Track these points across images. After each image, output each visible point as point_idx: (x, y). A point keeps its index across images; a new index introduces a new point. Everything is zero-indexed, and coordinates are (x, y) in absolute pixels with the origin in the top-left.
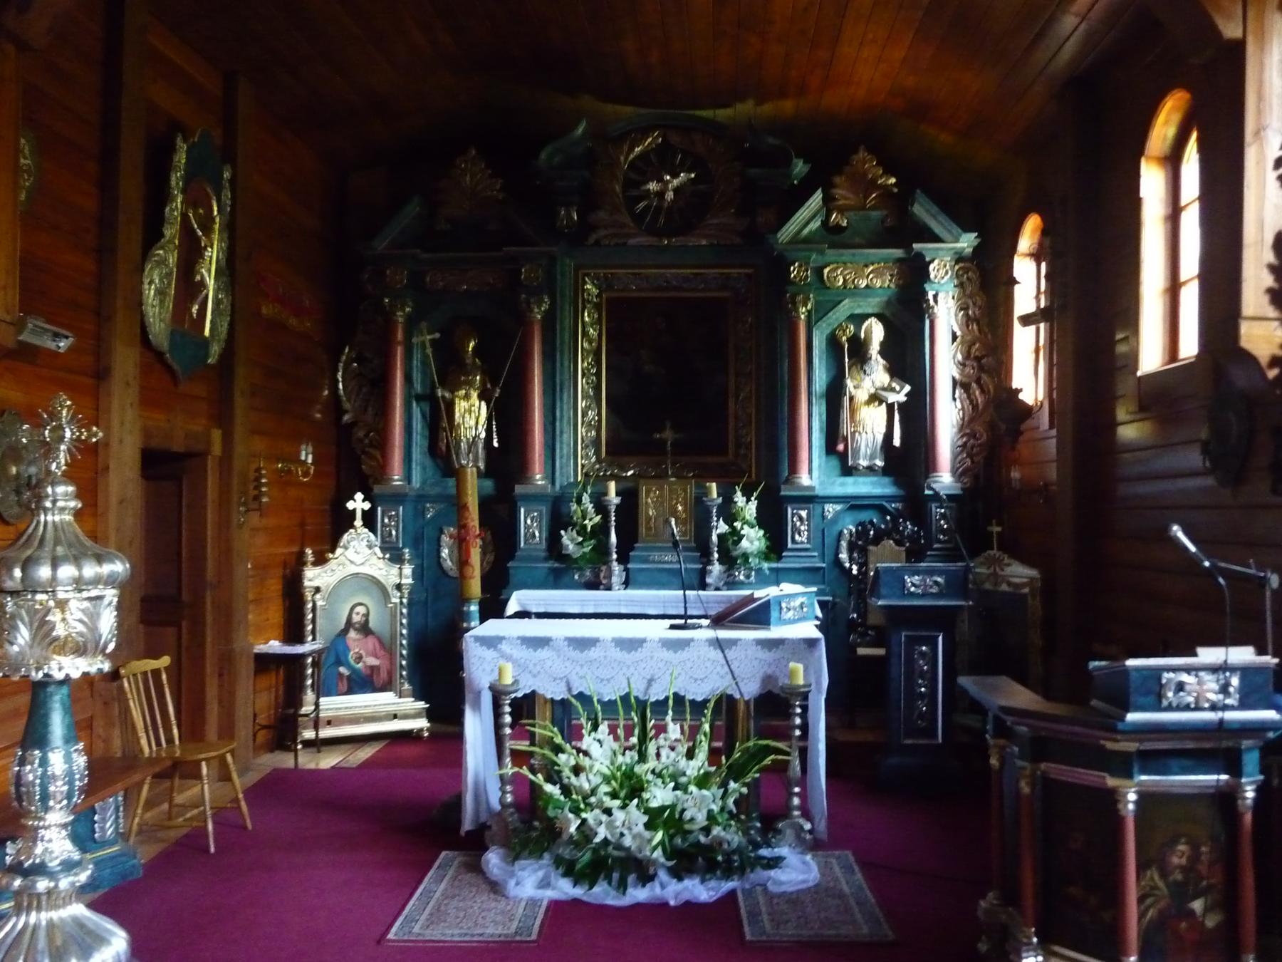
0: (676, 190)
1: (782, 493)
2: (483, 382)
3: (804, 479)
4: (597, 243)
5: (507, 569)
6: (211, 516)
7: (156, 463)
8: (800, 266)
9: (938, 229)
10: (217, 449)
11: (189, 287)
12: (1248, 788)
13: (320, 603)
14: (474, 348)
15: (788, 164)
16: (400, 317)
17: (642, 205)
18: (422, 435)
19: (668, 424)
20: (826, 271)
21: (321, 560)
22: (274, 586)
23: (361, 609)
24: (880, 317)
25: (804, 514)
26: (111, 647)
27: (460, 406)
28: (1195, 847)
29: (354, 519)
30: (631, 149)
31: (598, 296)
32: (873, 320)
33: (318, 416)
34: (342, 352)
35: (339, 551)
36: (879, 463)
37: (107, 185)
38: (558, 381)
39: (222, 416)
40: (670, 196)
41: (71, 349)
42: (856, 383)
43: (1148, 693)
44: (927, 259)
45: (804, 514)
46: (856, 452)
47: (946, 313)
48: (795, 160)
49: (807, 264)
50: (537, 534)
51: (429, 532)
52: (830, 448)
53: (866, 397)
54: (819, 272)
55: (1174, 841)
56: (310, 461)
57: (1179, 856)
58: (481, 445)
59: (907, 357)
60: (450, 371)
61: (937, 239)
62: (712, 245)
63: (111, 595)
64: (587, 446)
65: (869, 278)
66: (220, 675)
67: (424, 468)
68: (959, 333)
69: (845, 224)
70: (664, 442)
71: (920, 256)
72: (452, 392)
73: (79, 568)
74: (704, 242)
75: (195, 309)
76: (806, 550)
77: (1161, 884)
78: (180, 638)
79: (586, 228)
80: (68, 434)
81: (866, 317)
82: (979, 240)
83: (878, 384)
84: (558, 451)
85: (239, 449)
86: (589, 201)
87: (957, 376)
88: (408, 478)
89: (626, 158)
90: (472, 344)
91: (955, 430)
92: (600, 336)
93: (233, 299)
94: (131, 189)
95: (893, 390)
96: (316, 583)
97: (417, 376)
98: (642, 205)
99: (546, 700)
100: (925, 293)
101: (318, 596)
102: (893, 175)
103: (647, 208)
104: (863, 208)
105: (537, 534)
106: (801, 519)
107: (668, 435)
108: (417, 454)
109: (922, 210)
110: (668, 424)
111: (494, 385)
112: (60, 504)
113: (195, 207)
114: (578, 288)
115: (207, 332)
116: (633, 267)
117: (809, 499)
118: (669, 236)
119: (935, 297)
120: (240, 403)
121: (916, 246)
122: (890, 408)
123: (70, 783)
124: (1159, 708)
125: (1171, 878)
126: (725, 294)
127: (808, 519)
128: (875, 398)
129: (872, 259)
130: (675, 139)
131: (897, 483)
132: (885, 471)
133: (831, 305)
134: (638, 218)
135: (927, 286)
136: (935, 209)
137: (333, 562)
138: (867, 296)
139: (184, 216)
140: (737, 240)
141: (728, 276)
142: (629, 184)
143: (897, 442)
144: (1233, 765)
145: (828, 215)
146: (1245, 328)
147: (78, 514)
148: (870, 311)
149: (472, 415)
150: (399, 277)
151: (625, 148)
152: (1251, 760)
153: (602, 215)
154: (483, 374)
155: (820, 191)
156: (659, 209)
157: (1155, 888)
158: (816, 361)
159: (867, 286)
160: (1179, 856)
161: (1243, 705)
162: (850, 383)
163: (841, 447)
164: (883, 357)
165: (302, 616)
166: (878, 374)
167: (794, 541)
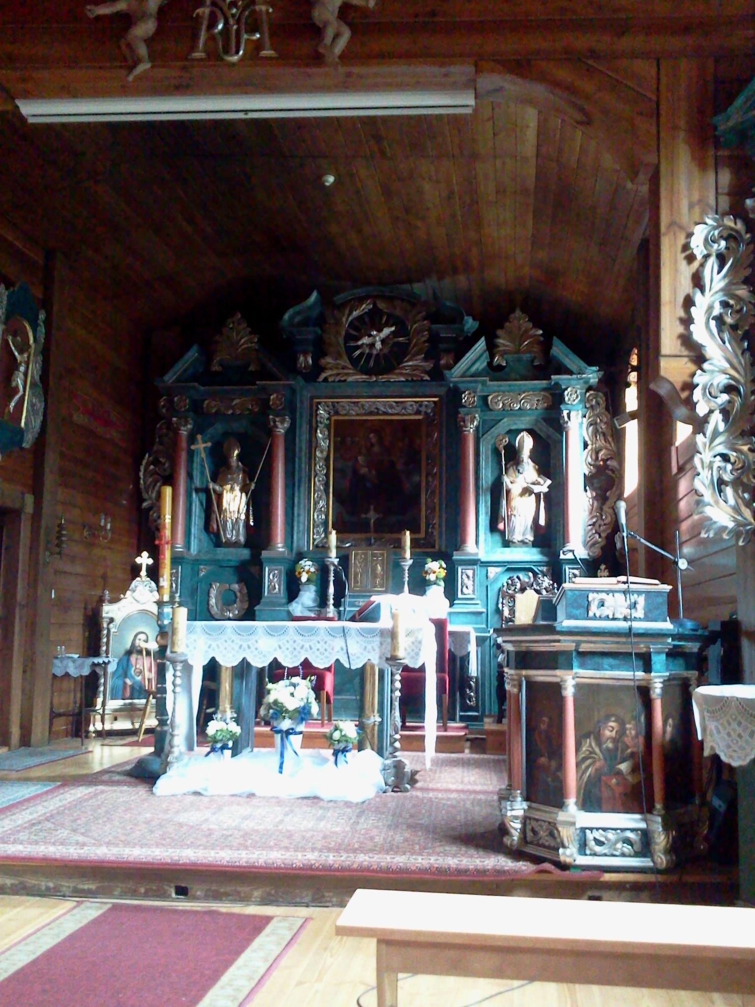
1: (454, 557)
2: (244, 480)
4: (326, 380)
5: (255, 611)
8: (470, 394)
9: (573, 367)
10: (29, 508)
12: (656, 680)
13: (113, 630)
14: (238, 455)
16: (184, 432)
17: (358, 352)
18: (200, 517)
20: (490, 398)
21: (115, 600)
22: (77, 617)
23: (142, 637)
24: (531, 432)
28: (622, 723)
29: (140, 570)
30: (350, 313)
31: (328, 419)
33: (124, 502)
34: (143, 458)
35: (128, 593)
40: (378, 345)
43: (579, 607)
44: (563, 387)
45: (470, 573)
46: (512, 531)
47: (578, 427)
48: (466, 318)
50: (277, 586)
51: (202, 587)
52: (493, 527)
53: (520, 490)
54: (484, 399)
55: (607, 718)
56: (109, 527)
57: (610, 731)
60: (220, 470)
64: (318, 526)
65: (524, 401)
67: (200, 540)
68: (589, 442)
69: (504, 364)
71: (557, 385)
72: (222, 486)
77: (597, 750)
79: (318, 368)
81: (519, 431)
82: (601, 373)
83: (530, 481)
84: (295, 528)
85: (46, 508)
86: (320, 350)
87: (587, 473)
88: (188, 545)
89: (347, 320)
90: (236, 452)
92: (329, 447)
95: (539, 484)
96: (110, 615)
97: (196, 474)
98: (358, 352)
100: (561, 412)
101: (111, 625)
102: (541, 328)
103: (362, 354)
104: (518, 352)
105: (277, 586)
106: (468, 577)
109: (559, 350)
111: (251, 480)
114: (313, 413)
116: (351, 397)
118: (377, 374)
119: (569, 415)
120: (50, 479)
122: (538, 496)
124: (587, 618)
125: (604, 746)
126: (420, 417)
128: (527, 491)
129: (524, 388)
130: (381, 305)
131: (542, 553)
132: (535, 544)
133: (494, 422)
134: (355, 362)
135: (562, 407)
136: (567, 350)
138: (520, 416)
140: (427, 378)
142: (348, 338)
143: (542, 522)
145: (492, 357)
146: (664, 363)
148: (523, 427)
149: (234, 502)
150: (182, 402)
151: (347, 312)
152: (659, 661)
153: (329, 360)
155: (483, 339)
156: (370, 355)
157: (593, 752)
161: (647, 618)
162: (506, 480)
163: (501, 526)
164: (533, 461)
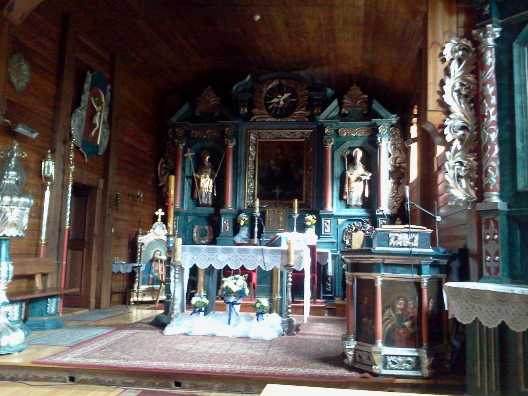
0: (284, 101)
2: (211, 172)
3: (329, 208)
4: (254, 120)
5: (216, 240)
6: (98, 210)
7: (78, 189)
9: (383, 114)
11: (90, 124)
13: (143, 249)
14: (209, 159)
15: (325, 90)
16: (181, 147)
19: (277, 186)
20: (340, 130)
21: (145, 234)
22: (125, 242)
24: (361, 148)
25: (329, 221)
26: (26, 228)
27: (203, 181)
28: (406, 301)
30: (267, 86)
32: (358, 149)
33: (150, 183)
34: (160, 161)
35: (151, 230)
36: (360, 203)
37: (58, 85)
38: (239, 172)
39: (105, 176)
40: (282, 103)
41: (36, 138)
42: (351, 173)
45: (329, 221)
46: (351, 200)
47: (386, 146)
48: (328, 89)
49: (332, 127)
53: (355, 178)
54: (337, 131)
55: (399, 298)
56: (142, 196)
57: (400, 305)
58: (210, 195)
59: (371, 163)
60: (199, 167)
61: (381, 117)
62: (296, 121)
63: (28, 210)
66: (98, 270)
67: (189, 203)
68: (392, 154)
69: (347, 113)
70: (275, 194)
71: (375, 124)
72: (200, 175)
73: (12, 198)
74: (294, 120)
75: (93, 132)
76: (329, 235)
77: (393, 315)
78: (83, 256)
79: (251, 114)
80: (15, 155)
81: (355, 148)
83: (360, 173)
85: (110, 187)
90: (208, 158)
91: (390, 191)
92: (256, 155)
93: (110, 133)
94: (68, 88)
95: (365, 175)
96: (142, 241)
98: (271, 107)
99: (202, 270)
103: (273, 107)
104: (355, 107)
106: (327, 223)
107: (278, 191)
108: (186, 198)
109: (376, 106)
110: (277, 186)
111: (215, 172)
112: (10, 177)
113: (95, 97)
114: (248, 138)
115: (98, 142)
117: (331, 216)
118: (281, 118)
120: (112, 170)
121: (373, 120)
123: (8, 274)
125: (397, 313)
126: (303, 140)
127: (330, 224)
128: (359, 179)
129: (358, 125)
130: (284, 82)
131: (367, 211)
132: (363, 207)
134: (269, 111)
137: (149, 234)
138: (356, 140)
139: (90, 102)
141: (303, 133)
142: (266, 99)
143: (367, 195)
144: (419, 269)
145: (341, 109)
147: (17, 182)
148: (356, 145)
149: (207, 183)
152: (426, 269)
153: (256, 110)
154: (212, 168)
156: (277, 108)
158: (336, 164)
159: (355, 136)
160: (400, 305)
161: (419, 247)
163: (345, 197)
164: (362, 163)
165: (136, 254)
166: (360, 169)
167: (325, 232)
